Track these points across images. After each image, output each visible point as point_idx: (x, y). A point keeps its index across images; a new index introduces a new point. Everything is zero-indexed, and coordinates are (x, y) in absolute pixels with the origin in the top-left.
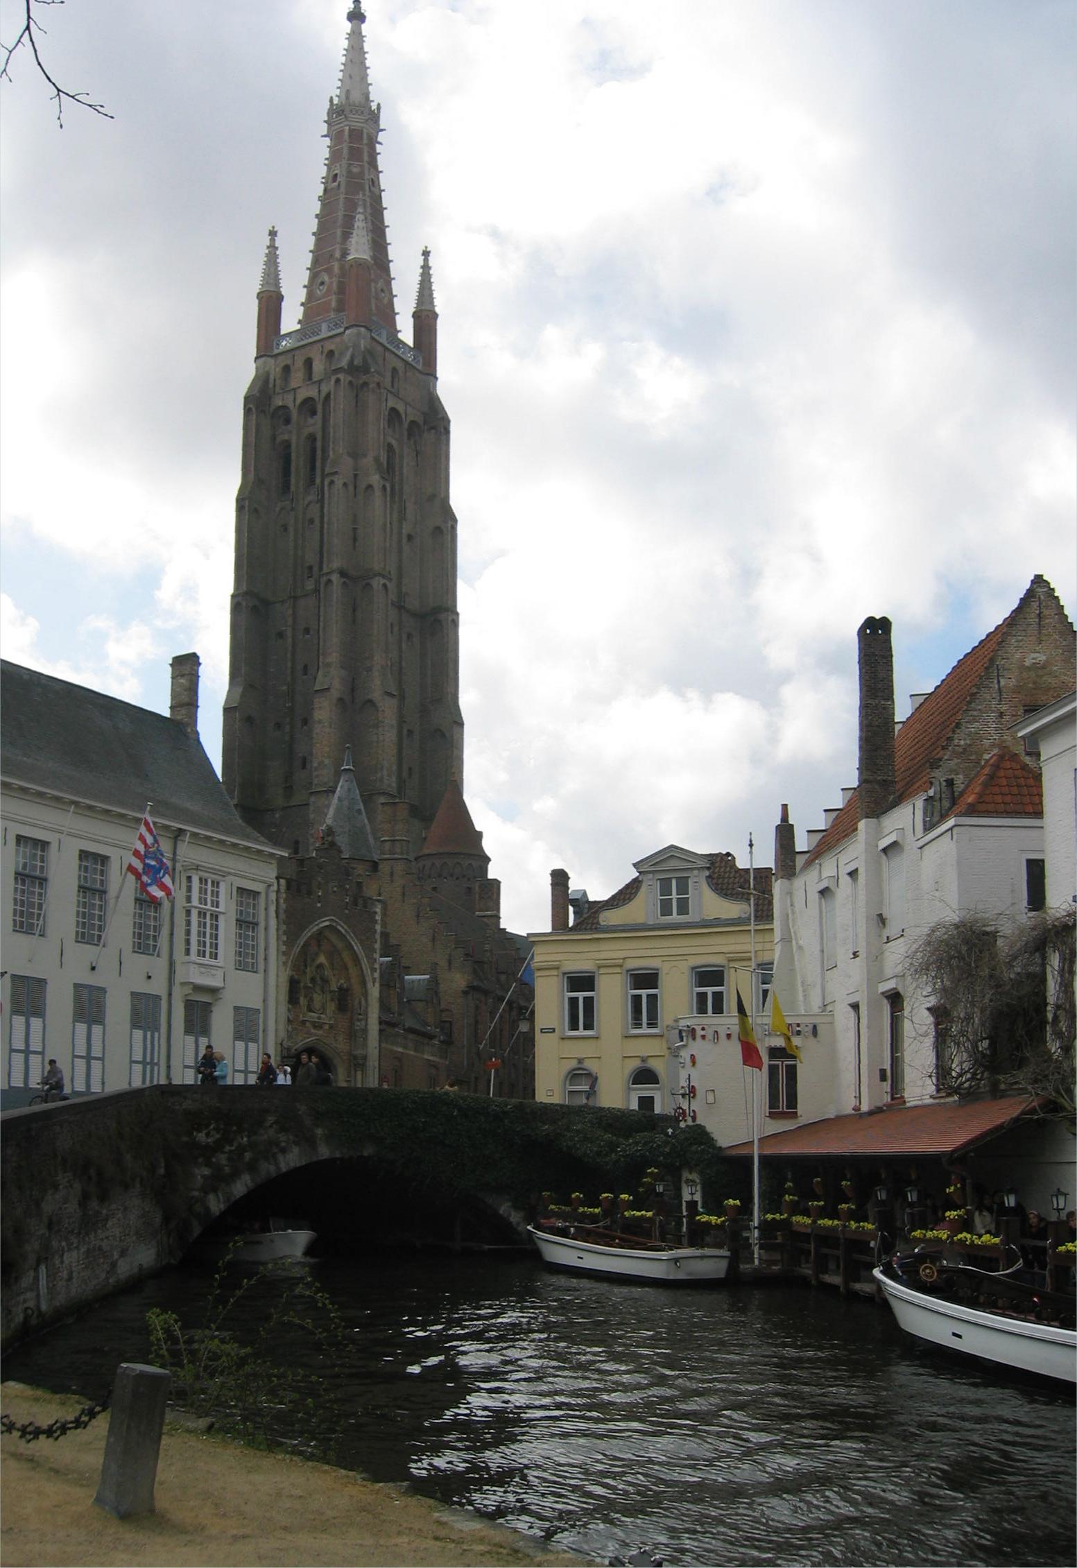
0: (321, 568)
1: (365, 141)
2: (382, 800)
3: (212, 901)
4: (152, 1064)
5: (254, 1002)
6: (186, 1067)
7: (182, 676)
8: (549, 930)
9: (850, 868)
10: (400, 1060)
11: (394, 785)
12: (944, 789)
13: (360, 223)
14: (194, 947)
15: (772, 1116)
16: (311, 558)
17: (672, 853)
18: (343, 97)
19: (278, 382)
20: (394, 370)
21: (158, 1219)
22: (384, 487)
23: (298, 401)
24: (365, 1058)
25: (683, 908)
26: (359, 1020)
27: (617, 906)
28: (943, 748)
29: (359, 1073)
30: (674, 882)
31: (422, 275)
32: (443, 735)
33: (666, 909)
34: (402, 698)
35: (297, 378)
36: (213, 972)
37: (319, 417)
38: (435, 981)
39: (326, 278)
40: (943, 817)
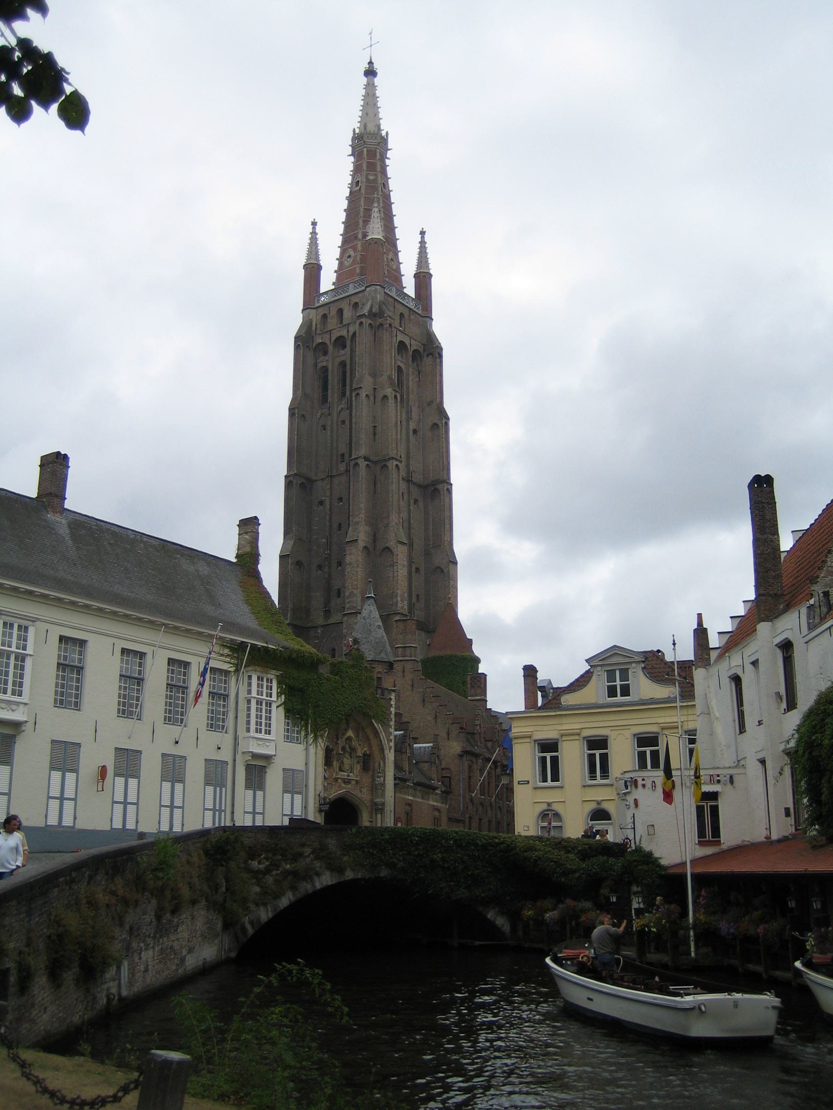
0: (350, 456)
1: (378, 157)
2: (397, 618)
3: (267, 693)
4: (220, 811)
5: (299, 765)
6: (245, 812)
7: (246, 533)
8: (523, 709)
9: (753, 659)
10: (410, 805)
11: (406, 607)
12: (822, 599)
13: (375, 214)
14: (253, 726)
15: (701, 843)
16: (343, 448)
17: (615, 651)
18: (363, 128)
19: (318, 326)
20: (402, 315)
21: (219, 926)
22: (396, 397)
23: (333, 339)
24: (383, 804)
25: (626, 691)
26: (379, 777)
27: (575, 691)
28: (819, 569)
29: (379, 816)
30: (618, 673)
31: (420, 248)
32: (442, 571)
33: (612, 692)
34: (411, 545)
35: (332, 322)
36: (267, 744)
37: (348, 349)
38: (436, 747)
39: (352, 253)
40: (823, 619)
